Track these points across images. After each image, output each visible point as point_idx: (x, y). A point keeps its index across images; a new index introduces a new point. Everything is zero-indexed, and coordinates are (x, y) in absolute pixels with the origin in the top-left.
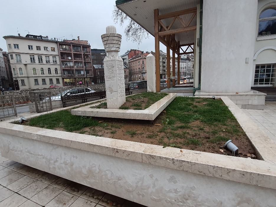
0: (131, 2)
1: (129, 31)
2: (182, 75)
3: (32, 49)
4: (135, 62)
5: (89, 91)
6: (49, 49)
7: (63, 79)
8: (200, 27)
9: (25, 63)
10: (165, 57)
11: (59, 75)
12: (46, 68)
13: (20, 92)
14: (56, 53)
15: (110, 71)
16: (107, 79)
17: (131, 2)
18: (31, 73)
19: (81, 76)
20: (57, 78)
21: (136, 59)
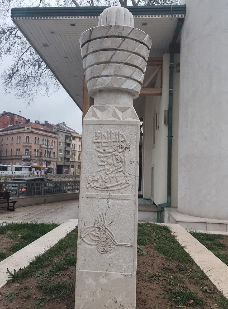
0: (46, 18)
1: (10, 77)
4: (10, 138)
5: (180, 306)
8: (170, 91)
10: (69, 135)
15: (110, 161)
16: (92, 193)
17: (46, 18)
21: (14, 131)
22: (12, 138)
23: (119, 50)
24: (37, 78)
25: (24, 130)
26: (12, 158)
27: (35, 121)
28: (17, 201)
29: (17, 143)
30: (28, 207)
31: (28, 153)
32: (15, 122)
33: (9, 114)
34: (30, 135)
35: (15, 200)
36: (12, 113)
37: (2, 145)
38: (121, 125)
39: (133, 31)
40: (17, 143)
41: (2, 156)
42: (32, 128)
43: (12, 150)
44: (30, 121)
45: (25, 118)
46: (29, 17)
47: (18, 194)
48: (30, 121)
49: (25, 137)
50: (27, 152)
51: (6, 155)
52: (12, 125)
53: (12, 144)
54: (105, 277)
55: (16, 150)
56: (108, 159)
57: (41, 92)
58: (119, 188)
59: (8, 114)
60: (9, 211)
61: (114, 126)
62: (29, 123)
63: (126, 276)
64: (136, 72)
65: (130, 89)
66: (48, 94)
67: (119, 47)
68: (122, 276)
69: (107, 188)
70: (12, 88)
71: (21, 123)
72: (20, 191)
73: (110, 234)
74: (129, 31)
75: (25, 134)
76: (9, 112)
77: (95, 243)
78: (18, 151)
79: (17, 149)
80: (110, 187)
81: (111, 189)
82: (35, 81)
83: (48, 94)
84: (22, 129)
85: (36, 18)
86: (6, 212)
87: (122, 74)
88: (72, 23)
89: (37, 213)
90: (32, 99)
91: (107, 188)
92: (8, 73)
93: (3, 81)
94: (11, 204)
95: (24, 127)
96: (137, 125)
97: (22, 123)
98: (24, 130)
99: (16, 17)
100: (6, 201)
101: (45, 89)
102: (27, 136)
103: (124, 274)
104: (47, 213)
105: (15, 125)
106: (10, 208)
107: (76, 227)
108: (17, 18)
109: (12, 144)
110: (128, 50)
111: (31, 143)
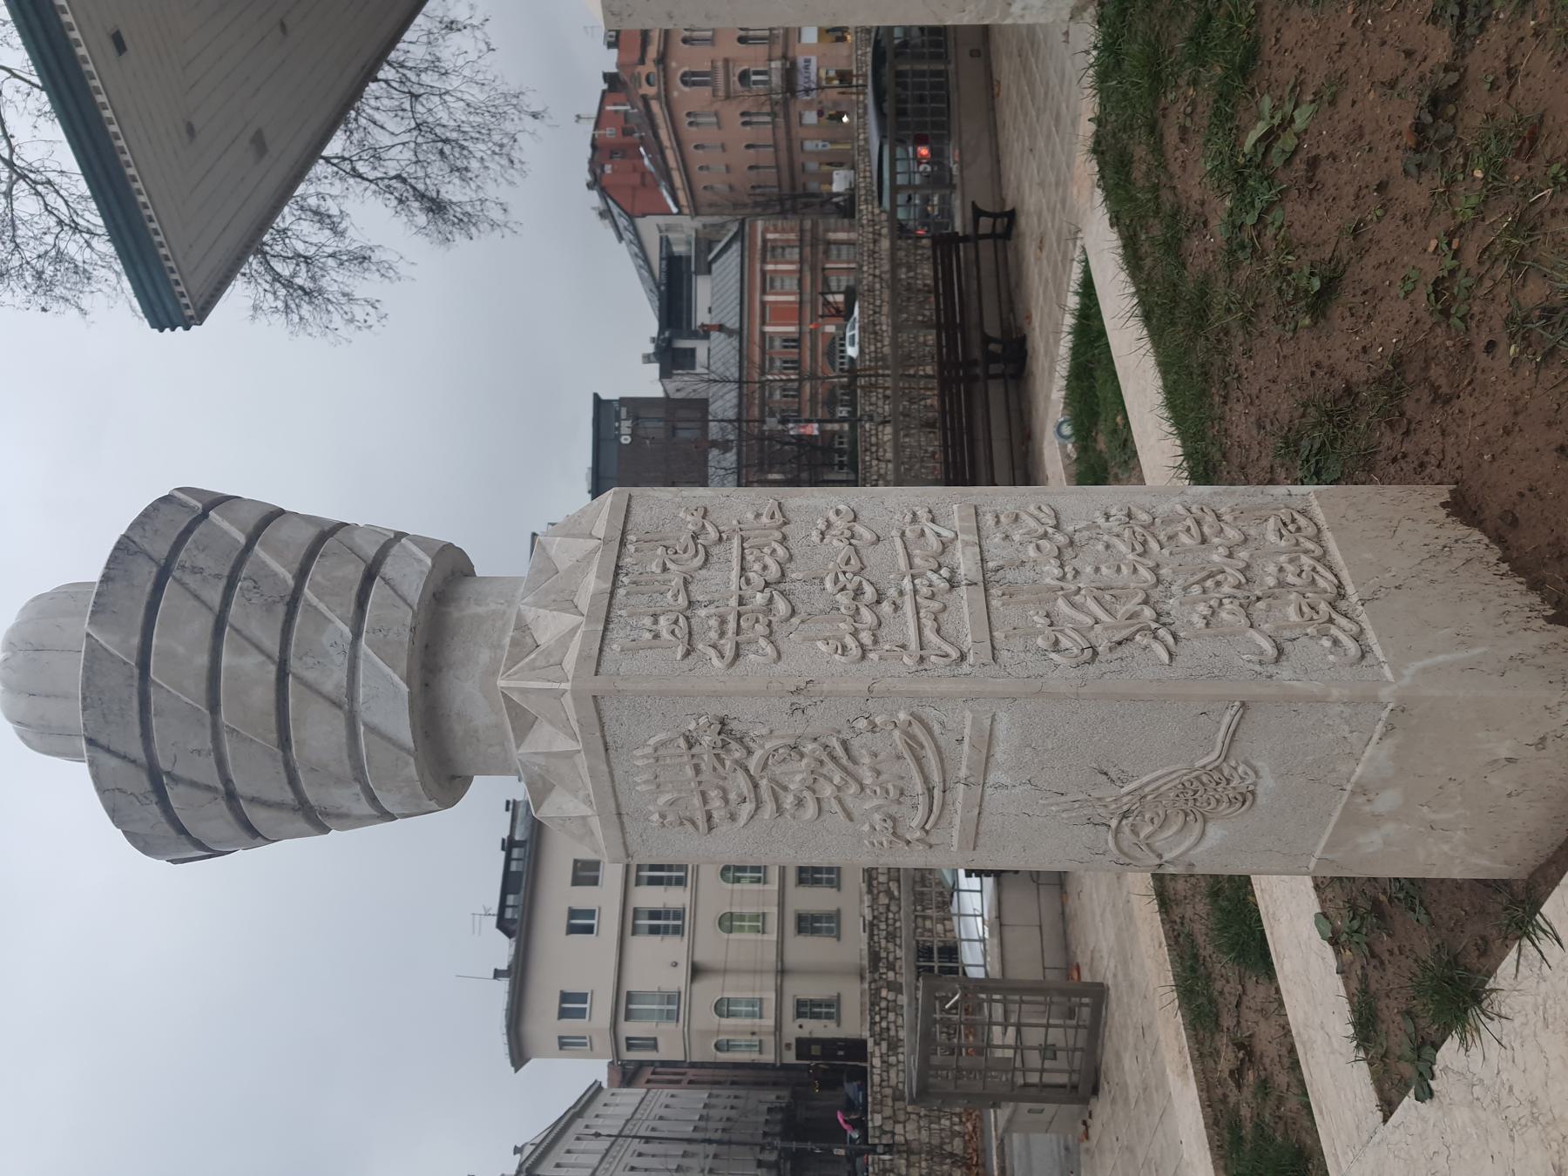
1: (436, 207)
3: (590, 914)
4: (697, 158)
9: (683, 971)
22: (696, 147)
23: (227, 781)
24: (414, 78)
25: (657, 97)
26: (783, 144)
27: (610, 45)
28: (973, 203)
29: (719, 125)
30: (1002, 142)
31: (757, 73)
32: (628, 140)
33: (595, 166)
34: (678, 67)
35: (969, 206)
36: (588, 152)
37: (731, 188)
38: (607, 750)
39: (103, 740)
40: (719, 125)
41: (780, 186)
42: (642, 61)
43: (748, 147)
44: (614, 70)
45: (604, 92)
46: (168, 271)
47: (940, 179)
48: (613, 69)
49: (687, 89)
50: (754, 78)
51: (772, 149)
52: (642, 149)
53: (723, 147)
54: (1371, 796)
55: (748, 128)
56: (785, 789)
57: (472, 56)
58: (930, 754)
59: (598, 171)
60: (1014, 232)
61: (618, 773)
62: (624, 77)
63: (1390, 728)
64: (310, 675)
65: (410, 693)
66: (475, 22)
67: (215, 790)
68: (1389, 743)
69: (930, 790)
70: (482, 201)
71: (626, 112)
72: (929, 169)
73: (1161, 782)
74: (114, 762)
75: (675, 94)
76: (586, 166)
77: (1197, 828)
78: (755, 119)
79: (744, 124)
80: (926, 779)
81: (936, 778)
82: (431, 91)
83: (473, 26)
84: (655, 107)
85: (157, 239)
86: (1016, 248)
87: (345, 756)
88: (110, 48)
89: (1034, 113)
90: (514, 101)
91: (930, 790)
92: (422, 219)
93: (459, 238)
94: (985, 225)
95: (645, 99)
96: (595, 697)
97: (628, 108)
98: (657, 97)
99: (183, 314)
100: (971, 245)
101: (455, 38)
102: (679, 82)
103: (1376, 737)
104: (1037, 63)
105: (641, 137)
106: (999, 229)
107: (1115, 229)
108: (187, 306)
109: (723, 147)
110: (210, 745)
111: (712, 62)
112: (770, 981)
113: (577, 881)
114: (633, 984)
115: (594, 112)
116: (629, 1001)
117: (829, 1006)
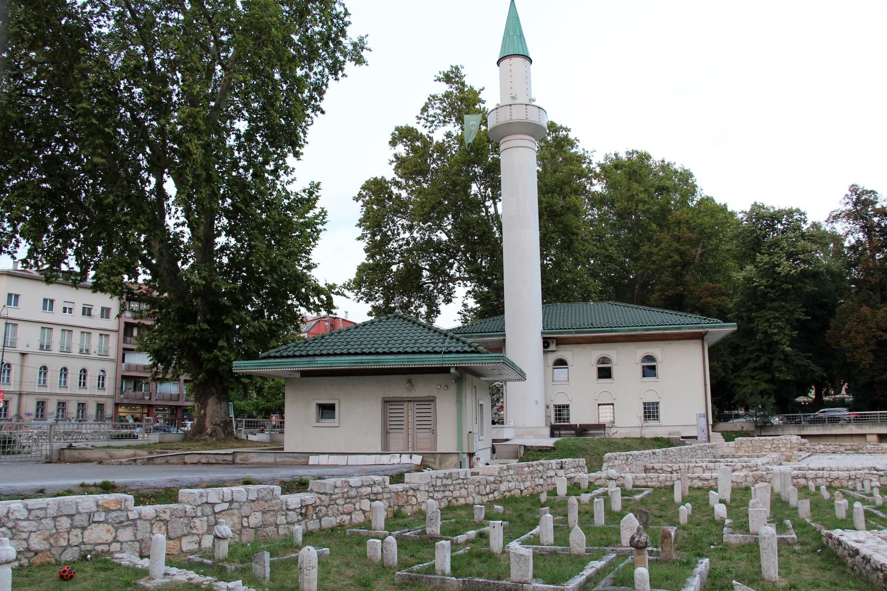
2: (555, 499)
3: (51, 309)
6: (97, 311)
7: (117, 405)
9: (24, 349)
11: (106, 393)
12: (55, 366)
13: (36, 437)
14: (112, 323)
18: (32, 384)
19: (171, 400)
20: (102, 400)
112: (17, 389)
113: (108, 317)
114: (21, 326)
115: (349, 319)
116: (13, 324)
117: (42, 416)
